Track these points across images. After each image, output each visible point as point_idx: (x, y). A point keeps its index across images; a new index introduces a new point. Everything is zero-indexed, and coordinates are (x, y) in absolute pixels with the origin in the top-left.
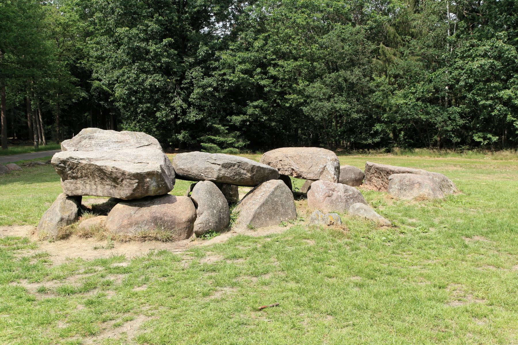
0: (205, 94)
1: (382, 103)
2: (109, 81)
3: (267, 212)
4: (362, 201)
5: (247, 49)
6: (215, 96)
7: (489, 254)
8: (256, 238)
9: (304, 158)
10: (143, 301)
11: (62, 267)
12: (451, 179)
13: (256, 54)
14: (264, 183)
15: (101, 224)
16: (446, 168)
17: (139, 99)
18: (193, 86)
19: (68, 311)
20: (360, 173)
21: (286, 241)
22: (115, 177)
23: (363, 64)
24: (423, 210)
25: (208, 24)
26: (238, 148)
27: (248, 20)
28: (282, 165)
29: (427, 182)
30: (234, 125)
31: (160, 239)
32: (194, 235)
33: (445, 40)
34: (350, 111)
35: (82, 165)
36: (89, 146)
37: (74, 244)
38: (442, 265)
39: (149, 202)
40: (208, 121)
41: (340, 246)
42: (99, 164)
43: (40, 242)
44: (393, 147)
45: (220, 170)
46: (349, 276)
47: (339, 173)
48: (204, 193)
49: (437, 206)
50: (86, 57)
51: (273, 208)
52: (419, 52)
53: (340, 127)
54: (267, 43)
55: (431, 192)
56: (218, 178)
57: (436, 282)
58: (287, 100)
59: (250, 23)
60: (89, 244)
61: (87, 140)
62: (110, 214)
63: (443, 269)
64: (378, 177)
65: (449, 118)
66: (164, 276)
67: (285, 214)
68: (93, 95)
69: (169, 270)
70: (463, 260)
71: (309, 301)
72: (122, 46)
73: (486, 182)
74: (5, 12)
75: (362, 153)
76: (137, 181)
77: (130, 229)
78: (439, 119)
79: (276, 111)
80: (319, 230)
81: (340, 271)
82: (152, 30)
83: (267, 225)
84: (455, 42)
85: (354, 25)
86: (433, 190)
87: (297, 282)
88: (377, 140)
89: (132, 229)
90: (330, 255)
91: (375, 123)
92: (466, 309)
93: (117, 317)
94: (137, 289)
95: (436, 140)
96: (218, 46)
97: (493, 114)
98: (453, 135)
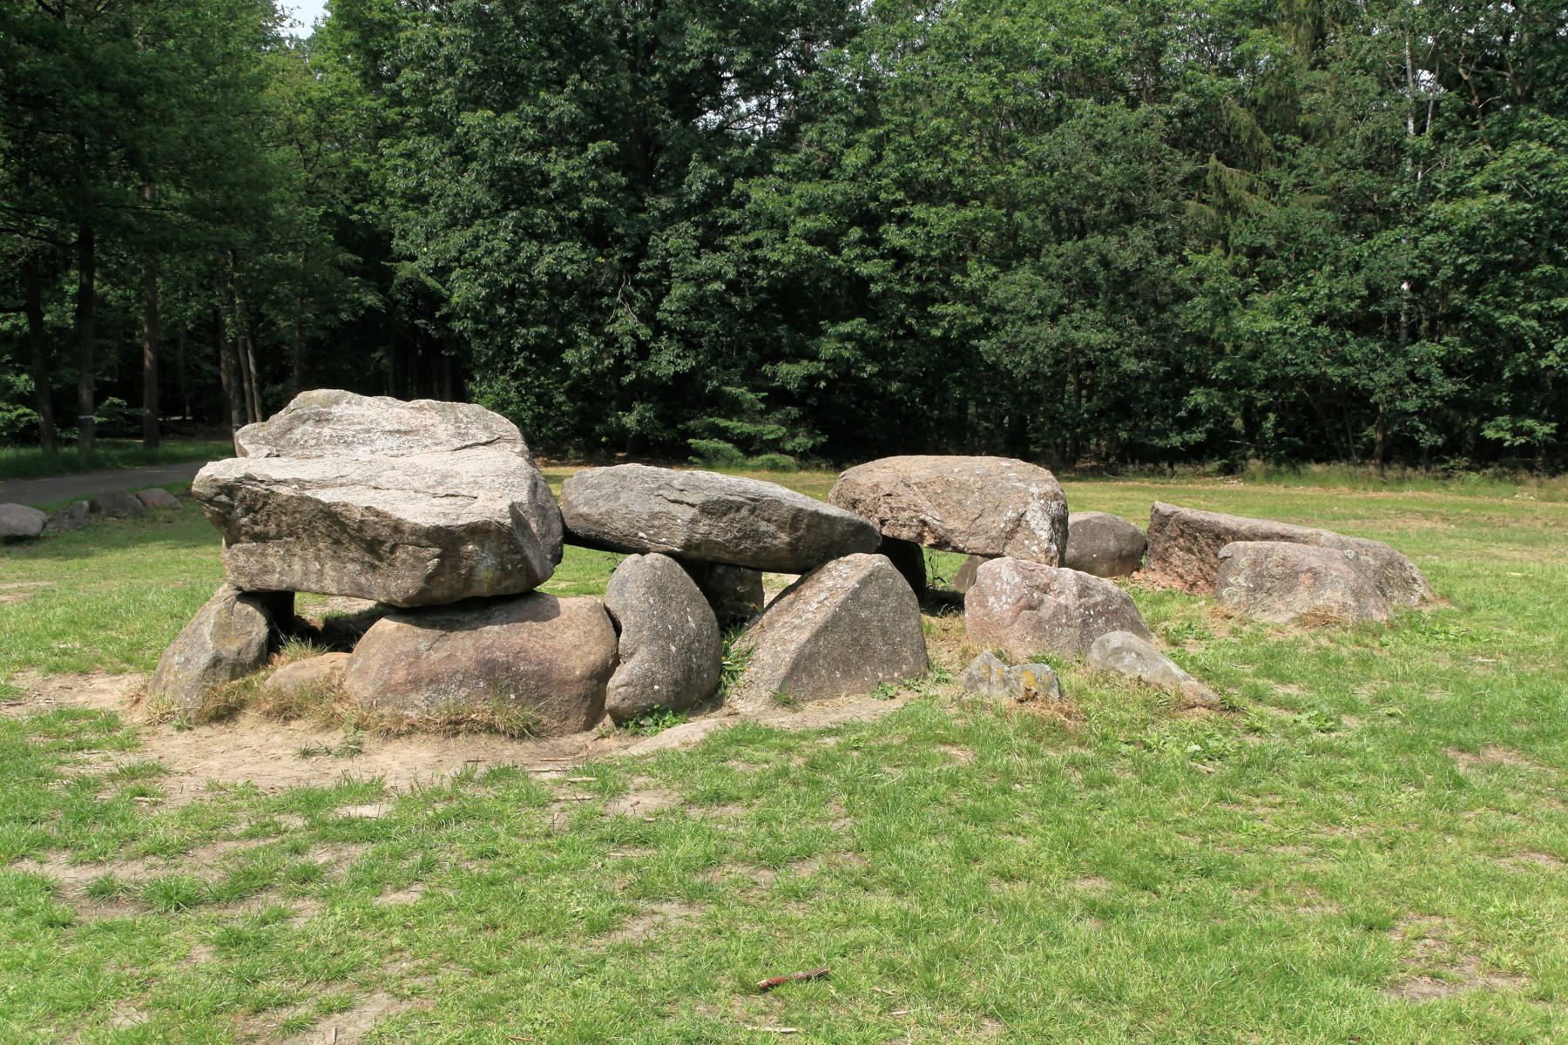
0: (702, 300)
1: (1212, 330)
2: (437, 260)
3: (835, 654)
4: (1136, 627)
5: (825, 175)
6: (731, 306)
7: (1537, 812)
8: (792, 737)
9: (958, 490)
10: (396, 941)
11: (186, 814)
12: (1412, 556)
13: (850, 188)
14: (831, 564)
15: (329, 680)
16: (1400, 524)
17: (519, 312)
18: (669, 277)
19: (161, 966)
20: (1135, 535)
21: (884, 748)
22: (374, 539)
23: (1159, 218)
24: (1323, 656)
25: (716, 106)
26: (792, 453)
27: (827, 89)
28: (891, 509)
29: (1338, 569)
30: (782, 389)
31: (502, 728)
32: (608, 719)
33: (1399, 148)
34: (1117, 352)
35: (280, 500)
36: (313, 442)
37: (251, 739)
38: (1380, 847)
39: (476, 615)
40: (710, 378)
41: (1051, 772)
42: (326, 496)
43: (149, 729)
44: (1244, 458)
45: (694, 521)
46: (1072, 874)
47: (1065, 535)
48: (642, 590)
49: (1366, 646)
50: (377, 194)
51: (856, 641)
52: (1325, 183)
53: (1089, 399)
54: (880, 158)
55: (1351, 602)
56: (689, 545)
57: (1358, 907)
58: (935, 320)
59: (835, 99)
60: (290, 738)
61: (309, 427)
62: (358, 647)
63: (1380, 861)
64: (1190, 551)
65: (1411, 375)
66: (483, 855)
67: (892, 661)
68: (398, 302)
69: (502, 836)
70: (1448, 830)
71: (929, 966)
72: (474, 164)
73: (1521, 570)
74: (151, 70)
75: (1151, 474)
76: (437, 551)
77: (413, 696)
78: (1382, 377)
79: (903, 350)
80: (990, 716)
81: (1043, 855)
82: (559, 118)
83: (835, 694)
84: (1432, 154)
85: (1133, 104)
86: (1357, 594)
87: (900, 894)
88: (1197, 436)
89: (419, 698)
90: (1018, 802)
91: (1190, 387)
92: (1458, 1009)
93: (302, 998)
94: (392, 899)
95: (1372, 441)
96: (743, 165)
97: (1543, 363)
98: (1422, 427)
